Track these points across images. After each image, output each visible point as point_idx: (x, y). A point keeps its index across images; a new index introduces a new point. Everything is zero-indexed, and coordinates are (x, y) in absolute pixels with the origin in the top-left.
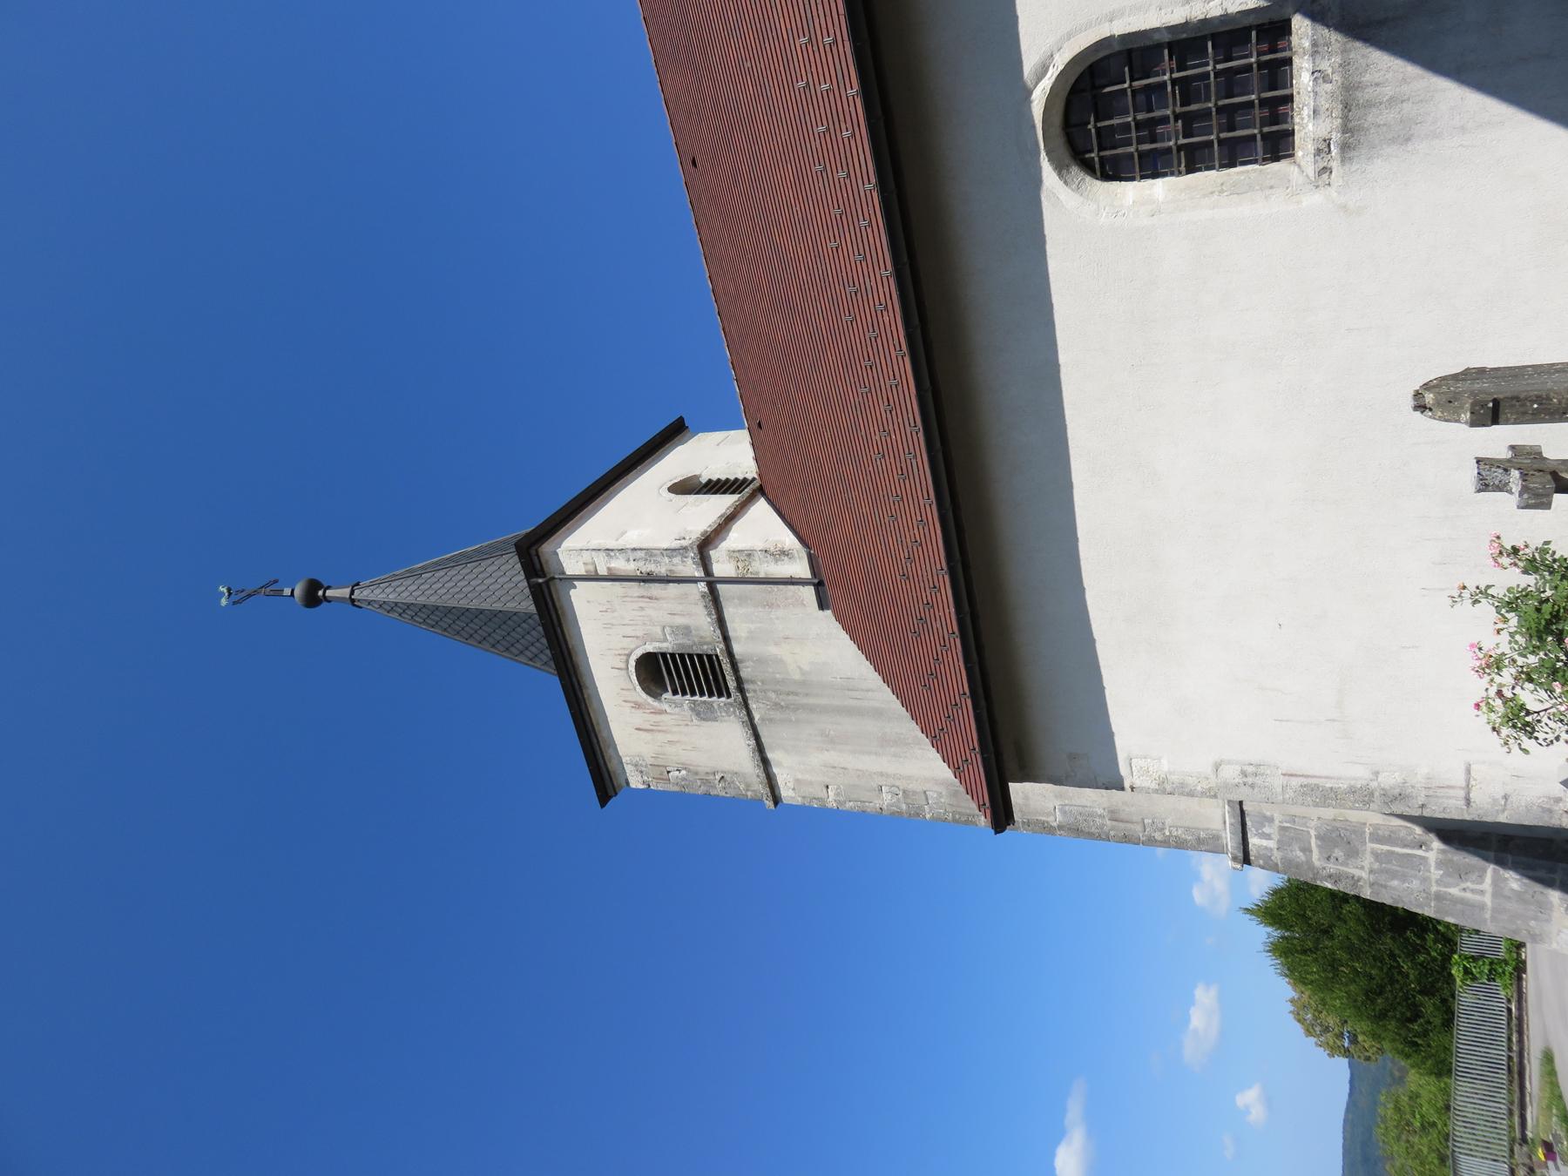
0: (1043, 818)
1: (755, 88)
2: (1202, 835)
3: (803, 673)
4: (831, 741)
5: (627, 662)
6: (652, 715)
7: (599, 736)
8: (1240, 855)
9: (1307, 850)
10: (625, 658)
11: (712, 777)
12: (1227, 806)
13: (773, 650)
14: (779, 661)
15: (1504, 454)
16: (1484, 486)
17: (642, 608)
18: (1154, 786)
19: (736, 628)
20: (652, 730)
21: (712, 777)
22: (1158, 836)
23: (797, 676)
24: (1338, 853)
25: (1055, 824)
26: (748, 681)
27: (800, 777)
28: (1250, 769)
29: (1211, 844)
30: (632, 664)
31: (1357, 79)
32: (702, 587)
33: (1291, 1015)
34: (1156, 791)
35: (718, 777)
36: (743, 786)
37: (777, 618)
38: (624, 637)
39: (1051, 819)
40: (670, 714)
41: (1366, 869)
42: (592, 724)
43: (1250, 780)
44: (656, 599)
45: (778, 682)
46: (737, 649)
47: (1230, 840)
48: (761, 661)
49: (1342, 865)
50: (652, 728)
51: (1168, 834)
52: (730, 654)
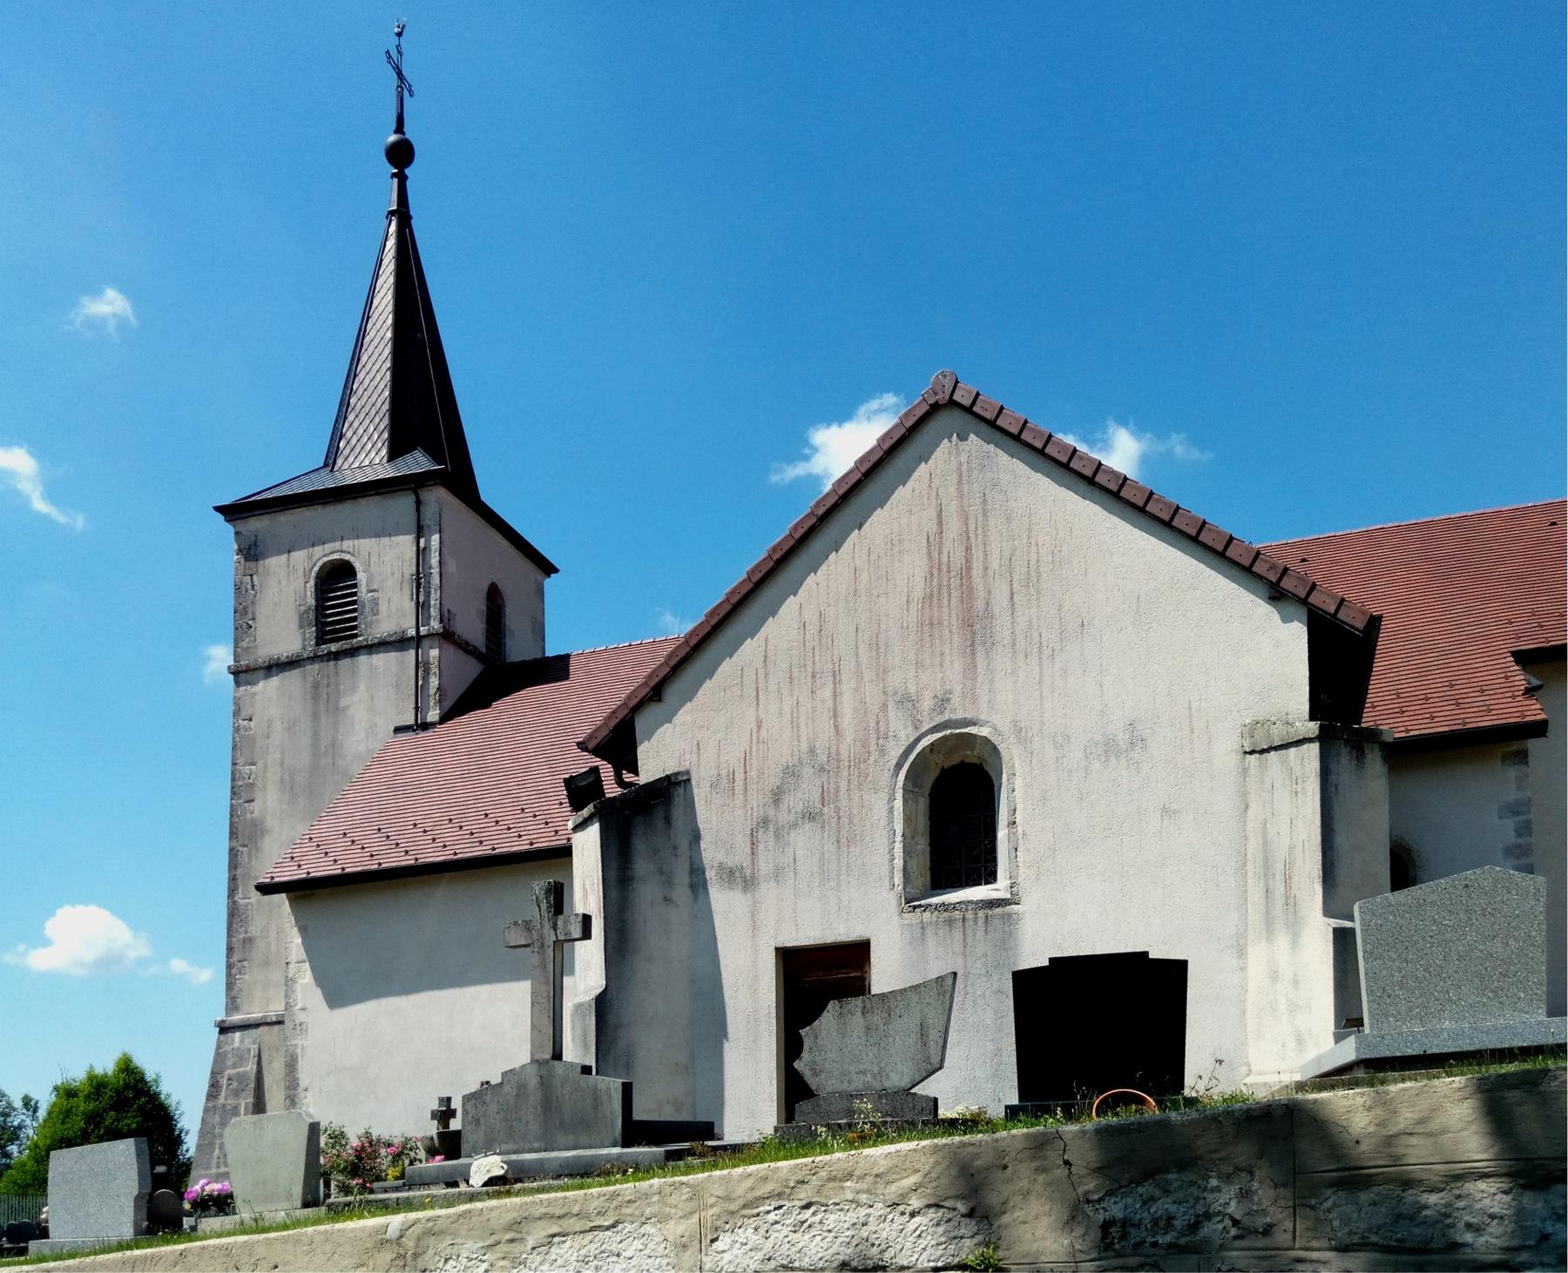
0: (240, 890)
1: (1449, 656)
2: (239, 1000)
3: (345, 709)
4: (291, 727)
5: (349, 553)
6: (302, 569)
7: (281, 513)
8: (226, 1025)
9: (235, 1066)
10: (351, 551)
11: (250, 616)
12: (261, 1015)
13: (362, 687)
14: (354, 689)
15: (453, 1107)
16: (441, 1100)
17: (393, 574)
18: (290, 976)
19: (380, 660)
20: (289, 566)
21: (250, 616)
22: (234, 971)
23: (342, 704)
24: (235, 1084)
25: (236, 898)
26: (336, 665)
27: (258, 697)
28: (304, 1027)
29: (232, 1004)
30: (347, 557)
31: (1100, 1152)
32: (412, 632)
33: (89, 1066)
34: (287, 977)
35: (250, 622)
36: (246, 645)
37: (388, 692)
38: (369, 553)
39: (240, 895)
40: (305, 587)
41: (226, 1102)
42: (292, 509)
43: (298, 1027)
44: (401, 588)
45: (337, 685)
46: (363, 659)
47: (237, 1018)
48: (353, 673)
49: (227, 1087)
50: (291, 566)
51: (237, 977)
52: (353, 652)
